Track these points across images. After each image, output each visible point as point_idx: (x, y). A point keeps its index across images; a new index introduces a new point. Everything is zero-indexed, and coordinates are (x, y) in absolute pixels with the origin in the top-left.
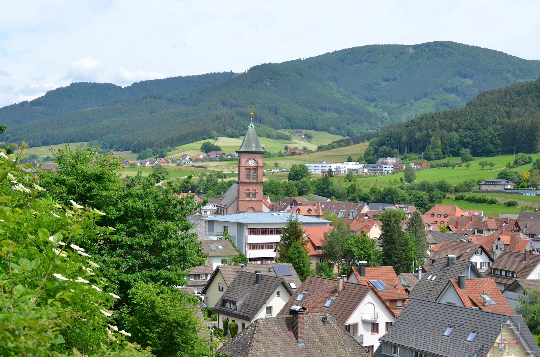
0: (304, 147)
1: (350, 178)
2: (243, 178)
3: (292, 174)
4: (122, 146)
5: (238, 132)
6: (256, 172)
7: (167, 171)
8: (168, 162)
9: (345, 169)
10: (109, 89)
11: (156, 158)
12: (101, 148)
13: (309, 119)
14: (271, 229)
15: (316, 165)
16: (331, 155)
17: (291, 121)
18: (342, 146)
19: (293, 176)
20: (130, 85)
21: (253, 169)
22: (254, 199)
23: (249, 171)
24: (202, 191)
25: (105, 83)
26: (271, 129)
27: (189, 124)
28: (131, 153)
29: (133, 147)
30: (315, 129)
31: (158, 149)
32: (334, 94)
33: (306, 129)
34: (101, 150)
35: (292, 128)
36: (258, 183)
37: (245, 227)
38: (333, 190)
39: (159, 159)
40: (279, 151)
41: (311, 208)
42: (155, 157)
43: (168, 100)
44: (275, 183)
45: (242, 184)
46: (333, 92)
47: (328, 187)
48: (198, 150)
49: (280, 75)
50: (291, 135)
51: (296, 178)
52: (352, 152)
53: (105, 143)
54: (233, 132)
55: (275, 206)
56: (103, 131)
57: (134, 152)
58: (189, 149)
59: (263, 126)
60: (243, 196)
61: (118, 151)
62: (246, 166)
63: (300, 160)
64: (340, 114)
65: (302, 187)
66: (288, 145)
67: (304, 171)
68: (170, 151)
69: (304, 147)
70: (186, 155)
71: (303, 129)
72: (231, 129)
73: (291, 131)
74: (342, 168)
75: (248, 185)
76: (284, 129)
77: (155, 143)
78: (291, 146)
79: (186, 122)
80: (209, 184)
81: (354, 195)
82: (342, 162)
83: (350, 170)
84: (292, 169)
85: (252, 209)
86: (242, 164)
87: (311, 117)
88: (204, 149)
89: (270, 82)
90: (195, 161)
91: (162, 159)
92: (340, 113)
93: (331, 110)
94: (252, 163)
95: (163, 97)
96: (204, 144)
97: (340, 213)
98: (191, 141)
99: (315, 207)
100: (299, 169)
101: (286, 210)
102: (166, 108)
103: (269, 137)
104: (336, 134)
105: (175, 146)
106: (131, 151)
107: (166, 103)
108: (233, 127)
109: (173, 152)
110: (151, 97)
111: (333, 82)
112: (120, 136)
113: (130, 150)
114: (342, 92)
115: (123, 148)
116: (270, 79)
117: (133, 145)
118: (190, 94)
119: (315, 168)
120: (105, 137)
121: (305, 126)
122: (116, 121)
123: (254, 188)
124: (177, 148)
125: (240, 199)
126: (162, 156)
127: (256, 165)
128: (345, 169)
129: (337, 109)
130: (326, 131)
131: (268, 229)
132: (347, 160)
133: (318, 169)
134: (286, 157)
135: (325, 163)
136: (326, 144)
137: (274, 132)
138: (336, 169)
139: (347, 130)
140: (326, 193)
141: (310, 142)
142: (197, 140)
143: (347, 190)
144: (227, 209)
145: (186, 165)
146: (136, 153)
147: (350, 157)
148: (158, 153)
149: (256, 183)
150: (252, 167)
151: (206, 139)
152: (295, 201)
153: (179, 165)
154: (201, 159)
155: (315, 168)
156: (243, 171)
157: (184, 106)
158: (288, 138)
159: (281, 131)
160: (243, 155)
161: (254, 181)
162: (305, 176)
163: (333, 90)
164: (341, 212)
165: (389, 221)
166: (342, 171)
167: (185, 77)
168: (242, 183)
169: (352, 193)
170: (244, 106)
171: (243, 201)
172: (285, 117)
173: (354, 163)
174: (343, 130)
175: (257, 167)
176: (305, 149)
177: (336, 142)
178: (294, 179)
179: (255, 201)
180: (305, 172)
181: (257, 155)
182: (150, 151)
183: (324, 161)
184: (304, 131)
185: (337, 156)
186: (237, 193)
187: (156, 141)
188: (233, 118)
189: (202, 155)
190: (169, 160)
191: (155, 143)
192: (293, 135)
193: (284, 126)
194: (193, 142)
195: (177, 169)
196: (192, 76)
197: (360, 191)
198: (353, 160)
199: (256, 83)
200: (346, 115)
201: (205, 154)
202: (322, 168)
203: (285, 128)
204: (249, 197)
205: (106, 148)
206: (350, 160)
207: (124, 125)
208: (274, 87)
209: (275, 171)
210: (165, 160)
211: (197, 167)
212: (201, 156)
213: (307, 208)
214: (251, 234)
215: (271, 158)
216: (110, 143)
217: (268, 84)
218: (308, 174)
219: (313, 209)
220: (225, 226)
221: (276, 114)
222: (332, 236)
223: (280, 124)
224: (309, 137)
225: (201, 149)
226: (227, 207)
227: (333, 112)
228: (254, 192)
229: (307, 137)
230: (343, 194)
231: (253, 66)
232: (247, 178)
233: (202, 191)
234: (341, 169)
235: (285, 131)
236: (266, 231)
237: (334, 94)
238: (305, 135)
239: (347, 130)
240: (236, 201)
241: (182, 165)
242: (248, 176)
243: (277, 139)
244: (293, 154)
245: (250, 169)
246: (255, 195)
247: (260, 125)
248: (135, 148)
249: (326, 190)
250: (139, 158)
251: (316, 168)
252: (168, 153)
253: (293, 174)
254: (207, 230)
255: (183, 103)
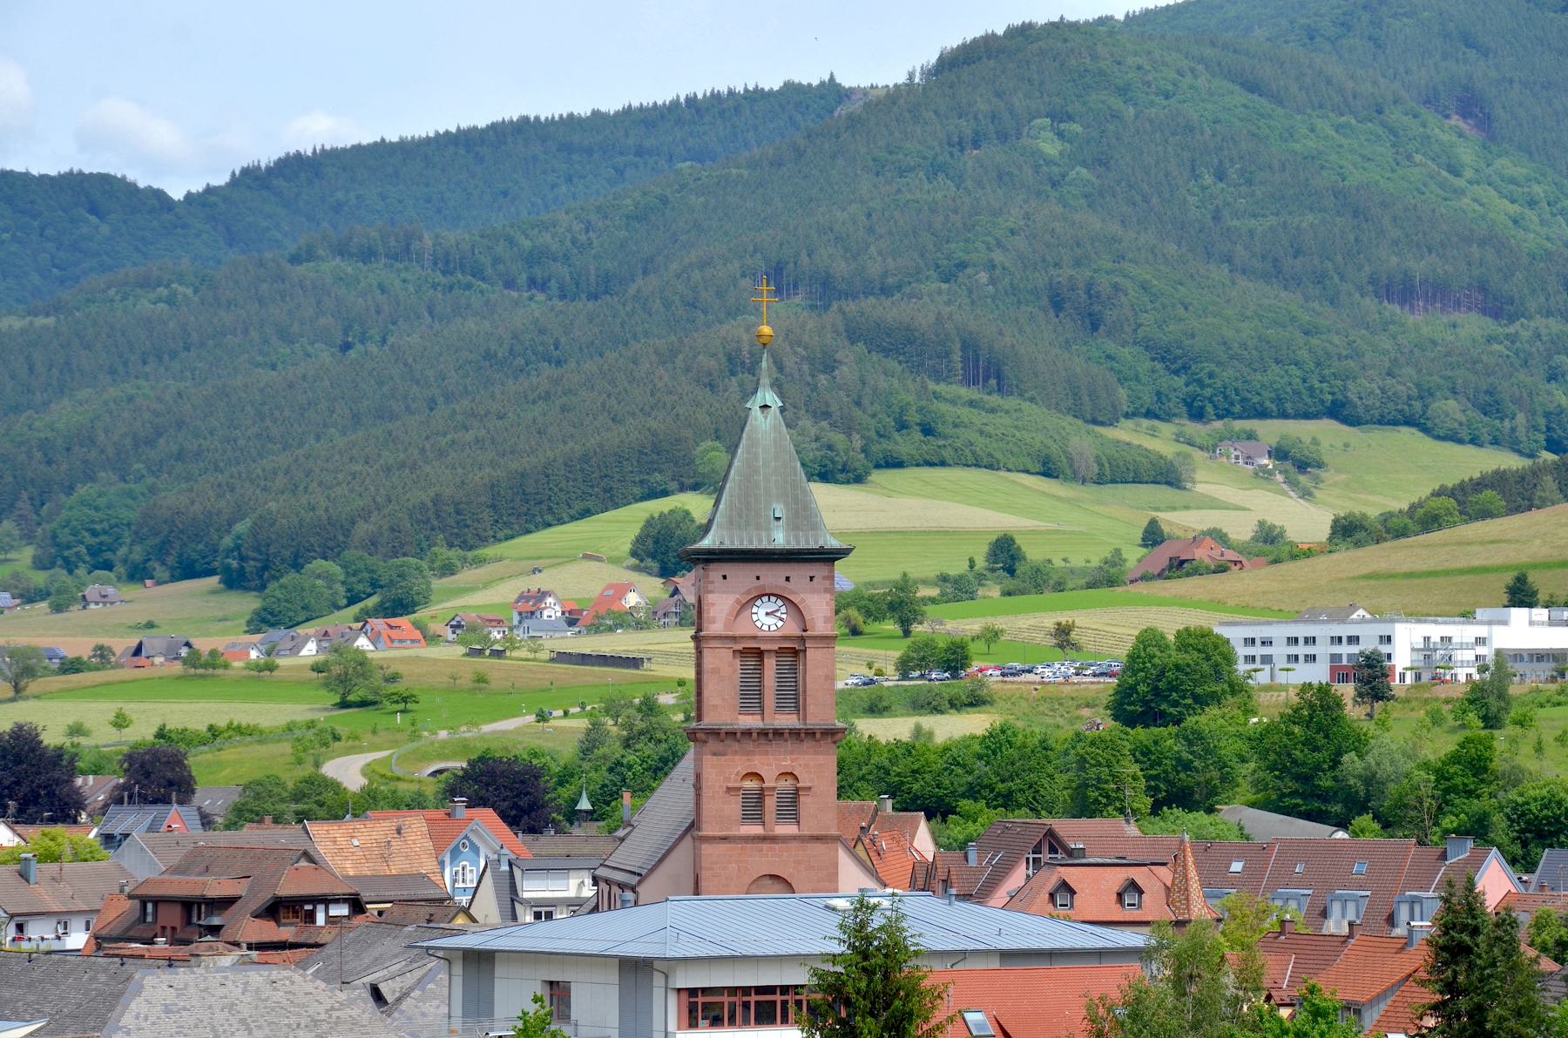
0: (1261, 524)
1: (1493, 704)
2: (723, 710)
3: (1133, 689)
4: (161, 551)
5: (858, 443)
6: (794, 669)
7: (399, 687)
8: (431, 639)
9: (1481, 650)
10: (94, 210)
11: (363, 617)
12: (40, 564)
13: (1303, 354)
14: (761, 990)
15: (1301, 631)
16: (1405, 568)
17: (1185, 368)
18: (1485, 514)
19: (1145, 703)
20: (221, 180)
21: (780, 652)
22: (789, 829)
23: (752, 662)
24: (585, 804)
25: (64, 169)
26: (1068, 422)
27: (564, 409)
28: (214, 592)
29: (228, 553)
30: (1339, 411)
31: (375, 561)
32: (1463, 192)
33: (1284, 415)
34: (40, 579)
35: (1197, 415)
36: (811, 734)
37: (658, 980)
38: (1369, 780)
39: (378, 623)
40: (1106, 553)
41: (1139, 875)
42: (356, 609)
43: (445, 262)
44: (1019, 740)
45: (713, 744)
46: (1460, 183)
47: (1335, 763)
48: (614, 561)
49: (1123, 91)
50: (1187, 456)
51: (1162, 714)
52: (1536, 550)
53: (64, 536)
54: (830, 447)
55: (941, 874)
56: (49, 463)
57: (235, 581)
58: (562, 559)
59: (1011, 402)
60: (723, 813)
61: (142, 580)
62: (734, 639)
63: (1182, 602)
64: (1496, 314)
65: (1187, 766)
66: (1162, 516)
67: (1205, 667)
68: (448, 570)
69: (1261, 524)
70: (542, 595)
71: (1263, 414)
72: (813, 431)
73: (1193, 428)
74: (1463, 646)
75: (749, 745)
76: (1145, 423)
77: (362, 530)
78: (1182, 521)
79: (547, 397)
80: (631, 758)
81: (1476, 805)
82: (1467, 616)
83: (1504, 664)
84: (1133, 657)
85: (778, 886)
86: (715, 627)
87: (1314, 341)
88: (653, 556)
89: (1061, 135)
90: (595, 628)
91: (394, 621)
92: (1497, 307)
93: (1439, 294)
94: (771, 621)
95: (416, 245)
96: (649, 523)
97: (1336, 908)
98: (578, 506)
99: (1165, 873)
100: (1177, 657)
101: (1001, 894)
102: (431, 313)
103: (1048, 470)
104: (1475, 441)
105: (483, 540)
106: (213, 581)
107: (435, 286)
108: (826, 415)
109: (465, 576)
110: (342, 250)
111: (1455, 120)
112: (153, 490)
113: (210, 573)
114: (1513, 181)
115: (171, 560)
116: (1059, 116)
117: (227, 541)
118: (577, 227)
119: (1293, 650)
120: (63, 497)
121: (1279, 400)
122: (131, 399)
123: (787, 763)
124: (489, 551)
125: (707, 831)
126: (400, 606)
127: (794, 630)
128: (1481, 650)
129: (1483, 288)
130: (1409, 422)
131: (746, 990)
132: (1505, 598)
133: (1312, 658)
134: (1143, 588)
135: (1363, 621)
136: (1399, 503)
137: (1083, 441)
138: (1427, 650)
139: (1547, 415)
140: (1325, 797)
141: (1306, 494)
142: (612, 500)
143: (1437, 771)
144: (633, 889)
145: (523, 653)
146: (247, 589)
147: (1521, 580)
148: (375, 585)
149: (795, 734)
150: (772, 639)
151: (665, 493)
152: (1053, 842)
153: (480, 652)
154: (631, 612)
155: (1293, 650)
156: (724, 666)
157: (540, 297)
158: (1168, 476)
159: (1126, 433)
160: (716, 571)
161: (788, 721)
162: (1215, 698)
163: (1455, 171)
164: (1345, 902)
165: (1464, 928)
166: (1463, 664)
167: (551, 122)
168: (715, 733)
169: (1470, 793)
170: (899, 287)
171: (724, 839)
172: (1148, 345)
173: (1541, 614)
174: (1521, 418)
175: (802, 639)
176: (1269, 537)
177: (1452, 493)
178: (1151, 717)
179: (794, 838)
180: (1217, 674)
181: (800, 573)
182: (329, 578)
183: (1353, 607)
184: (1271, 431)
185: (1447, 573)
186: (692, 806)
187: (365, 515)
188: (829, 366)
189: (643, 591)
190: (436, 627)
191: (362, 530)
192: (1198, 455)
193: (1148, 399)
194: (585, 513)
195: (466, 681)
196: (596, 114)
197: (1514, 778)
198: (1542, 596)
199: (976, 144)
200: (1539, 322)
201: (658, 582)
202: (1337, 649)
203: (1150, 414)
204: (759, 818)
205: (70, 567)
206: (1521, 595)
207: (180, 424)
208: (1084, 164)
209: (1055, 671)
210: (418, 625)
211: (584, 659)
212: (632, 599)
213: (1118, 877)
214: (693, 1024)
215: (1048, 596)
216: (94, 533)
217: (1050, 147)
218: (1236, 688)
219: (1153, 881)
220: (551, 983)
221: (1095, 327)
222: (1135, 1016)
223: (1122, 393)
224: (1302, 466)
225: (634, 554)
226: (634, 880)
227: (1458, 304)
228: (787, 784)
229: (1288, 465)
230: (1411, 800)
231: (954, 42)
232: (745, 708)
233: (585, 804)
234: (1460, 656)
235: (1153, 433)
236: (784, 1003)
237: (1463, 192)
238: (1279, 454)
239: (1547, 415)
240: (688, 842)
241: (498, 654)
242: (752, 696)
243: (1100, 481)
244: (1179, 567)
245: (760, 654)
246: (791, 806)
247: (995, 400)
248: (242, 558)
249: (1325, 782)
250: (263, 621)
251: (1301, 650)
252: (438, 584)
253: (1142, 688)
254: (457, 1010)
255: (532, 282)
